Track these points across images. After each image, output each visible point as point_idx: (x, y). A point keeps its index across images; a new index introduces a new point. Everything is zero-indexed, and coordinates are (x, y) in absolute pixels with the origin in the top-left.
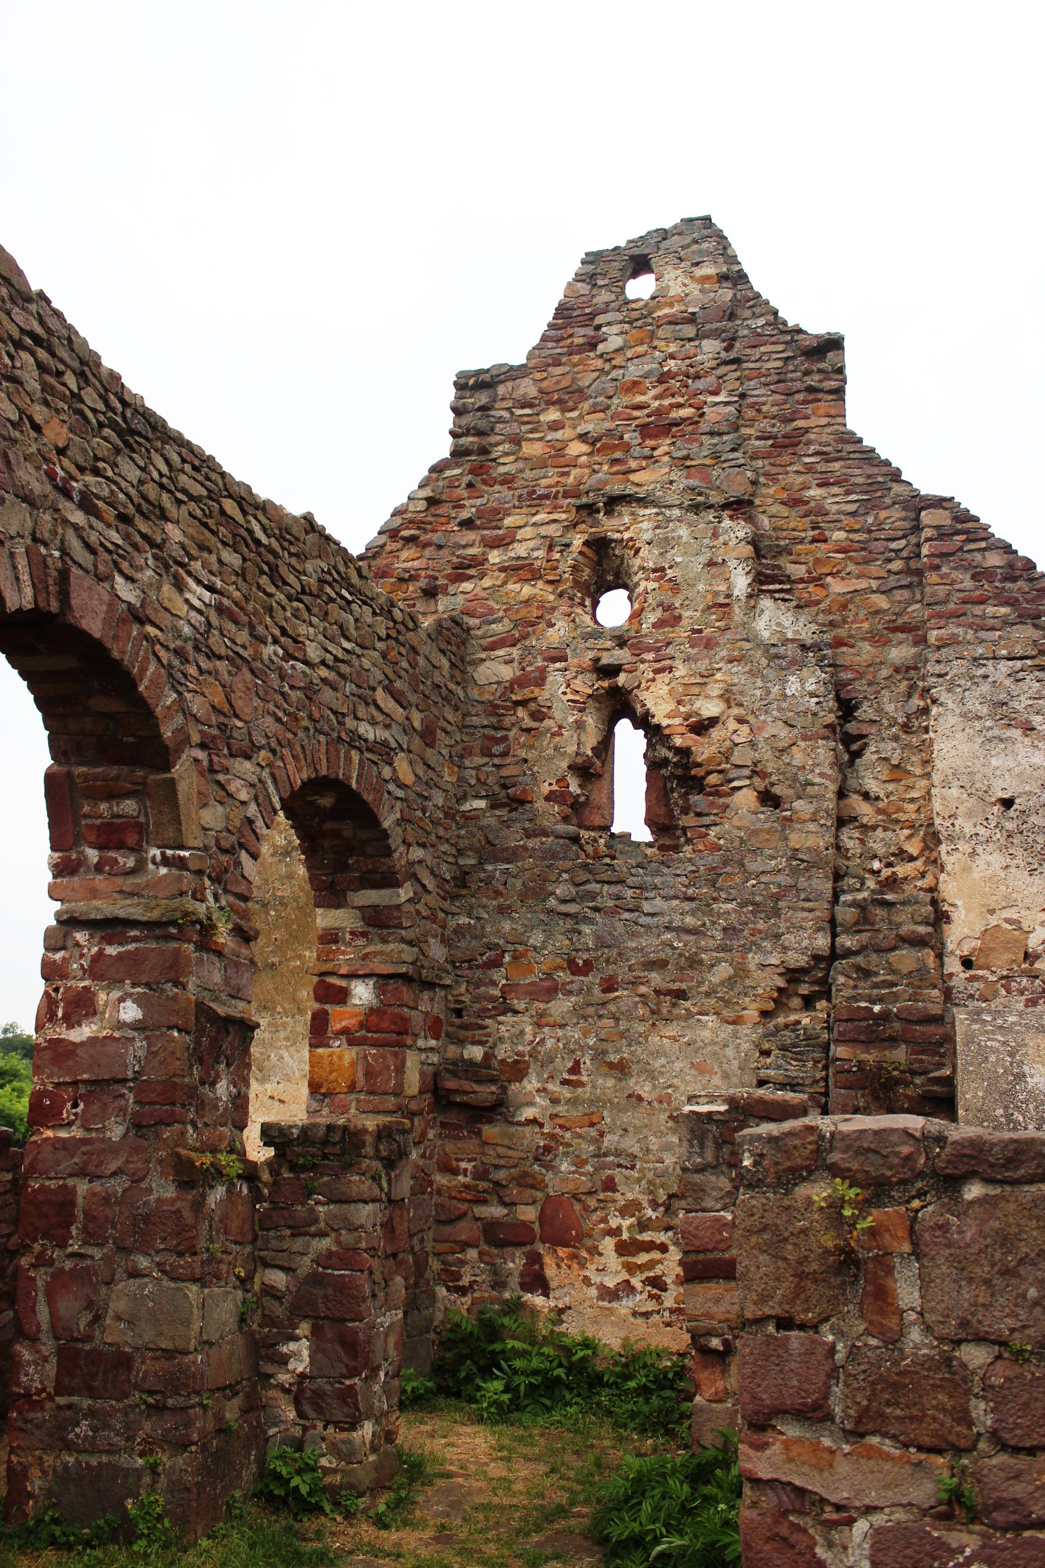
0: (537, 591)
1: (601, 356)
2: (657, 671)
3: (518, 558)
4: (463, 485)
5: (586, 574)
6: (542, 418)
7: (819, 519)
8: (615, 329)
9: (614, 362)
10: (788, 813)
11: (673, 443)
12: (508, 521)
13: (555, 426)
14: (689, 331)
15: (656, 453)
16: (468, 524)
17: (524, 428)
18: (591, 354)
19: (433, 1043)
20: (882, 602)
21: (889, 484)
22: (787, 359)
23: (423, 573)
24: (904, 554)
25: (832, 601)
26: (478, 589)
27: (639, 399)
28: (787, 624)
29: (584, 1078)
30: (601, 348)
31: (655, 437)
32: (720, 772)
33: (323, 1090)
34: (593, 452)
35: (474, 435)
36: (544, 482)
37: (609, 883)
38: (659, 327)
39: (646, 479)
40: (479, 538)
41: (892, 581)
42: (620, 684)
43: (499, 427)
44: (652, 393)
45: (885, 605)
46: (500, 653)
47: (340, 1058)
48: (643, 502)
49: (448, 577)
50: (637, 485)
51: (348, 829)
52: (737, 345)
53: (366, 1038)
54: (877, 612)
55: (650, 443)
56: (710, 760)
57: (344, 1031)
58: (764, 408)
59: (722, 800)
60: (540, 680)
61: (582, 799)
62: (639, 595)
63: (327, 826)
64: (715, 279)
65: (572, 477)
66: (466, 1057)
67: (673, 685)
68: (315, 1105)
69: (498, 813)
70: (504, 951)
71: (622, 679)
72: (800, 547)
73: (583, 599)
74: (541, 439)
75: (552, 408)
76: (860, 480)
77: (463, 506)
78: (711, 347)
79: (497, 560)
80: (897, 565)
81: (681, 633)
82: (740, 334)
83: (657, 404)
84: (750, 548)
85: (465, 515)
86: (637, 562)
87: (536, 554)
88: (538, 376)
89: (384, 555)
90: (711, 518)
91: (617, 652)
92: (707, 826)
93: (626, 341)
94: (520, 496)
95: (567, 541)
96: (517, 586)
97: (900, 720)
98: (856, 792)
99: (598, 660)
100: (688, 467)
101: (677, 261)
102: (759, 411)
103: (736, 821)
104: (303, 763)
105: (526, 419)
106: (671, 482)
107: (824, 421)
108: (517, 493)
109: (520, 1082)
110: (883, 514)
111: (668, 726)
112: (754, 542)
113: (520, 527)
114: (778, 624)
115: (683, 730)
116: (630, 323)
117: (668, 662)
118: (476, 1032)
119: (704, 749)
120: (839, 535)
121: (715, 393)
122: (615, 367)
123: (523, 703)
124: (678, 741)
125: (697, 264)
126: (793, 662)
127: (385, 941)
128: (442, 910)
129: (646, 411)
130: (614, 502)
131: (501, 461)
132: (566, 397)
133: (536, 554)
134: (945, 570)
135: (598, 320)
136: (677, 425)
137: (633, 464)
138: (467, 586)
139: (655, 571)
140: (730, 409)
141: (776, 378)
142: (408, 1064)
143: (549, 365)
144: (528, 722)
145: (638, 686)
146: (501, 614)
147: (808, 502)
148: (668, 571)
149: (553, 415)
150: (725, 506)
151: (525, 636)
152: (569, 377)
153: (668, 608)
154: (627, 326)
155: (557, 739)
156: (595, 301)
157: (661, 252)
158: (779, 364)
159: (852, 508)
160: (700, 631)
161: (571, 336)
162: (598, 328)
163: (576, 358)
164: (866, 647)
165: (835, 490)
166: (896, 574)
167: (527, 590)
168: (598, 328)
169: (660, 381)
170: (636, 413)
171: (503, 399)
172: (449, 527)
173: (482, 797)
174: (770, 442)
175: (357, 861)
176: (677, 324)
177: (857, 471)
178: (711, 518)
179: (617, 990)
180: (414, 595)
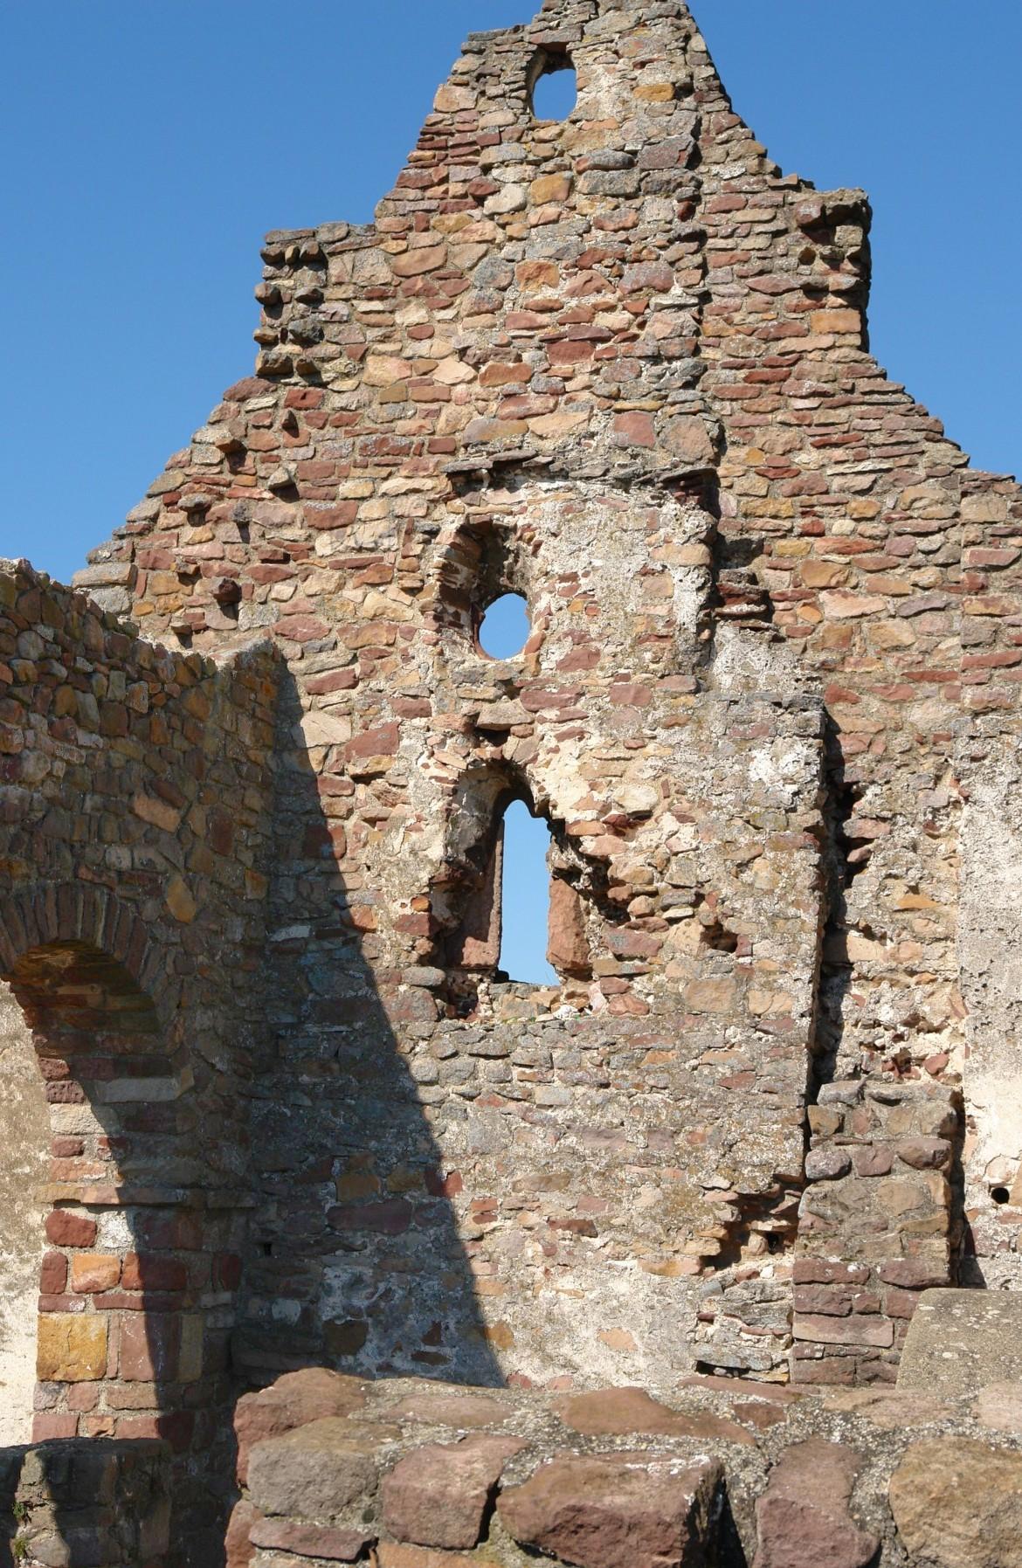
0: (388, 602)
1: (491, 217)
2: (561, 737)
3: (360, 550)
4: (277, 425)
5: (463, 576)
6: (398, 318)
7: (814, 500)
8: (511, 173)
9: (510, 230)
10: (747, 960)
11: (597, 372)
12: (346, 488)
13: (420, 333)
14: (628, 181)
15: (569, 386)
16: (286, 491)
17: (372, 334)
18: (477, 213)
19: (225, 1297)
20: (902, 632)
21: (927, 445)
22: (777, 234)
23: (216, 565)
24: (940, 558)
25: (828, 630)
26: (300, 595)
27: (547, 294)
28: (758, 666)
29: (447, 1351)
30: (490, 203)
31: (570, 357)
32: (653, 894)
33: (58, 1377)
34: (475, 378)
35: (294, 342)
36: (401, 426)
37: (487, 1057)
38: (580, 173)
39: (551, 432)
40: (301, 513)
41: (918, 600)
42: (507, 756)
43: (330, 331)
44: (567, 285)
45: (907, 638)
46: (334, 697)
47: (84, 1328)
48: (544, 471)
49: (254, 573)
50: (541, 437)
51: (92, 994)
52: (700, 209)
53: (123, 1299)
54: (897, 648)
55: (562, 367)
56: (636, 875)
57: (93, 1290)
58: (737, 317)
59: (654, 936)
60: (390, 743)
61: (454, 924)
62: (540, 614)
63: (62, 991)
64: (669, 94)
65: (443, 418)
66: (276, 1316)
67: (585, 758)
68: (46, 1400)
69: (327, 945)
70: (334, 1157)
71: (510, 748)
72: (783, 542)
73: (457, 615)
74: (397, 354)
75: (414, 301)
76: (878, 438)
77: (277, 460)
78: (659, 210)
79: (328, 551)
80: (928, 575)
81: (599, 678)
82: (705, 188)
83: (574, 302)
84: (703, 548)
85: (279, 477)
86: (537, 563)
87: (386, 543)
88: (394, 246)
89: (157, 531)
90: (648, 499)
91: (506, 705)
92: (631, 977)
93: (526, 194)
94: (364, 448)
95: (434, 526)
96: (359, 593)
97: (921, 818)
98: (856, 927)
99: (477, 715)
100: (619, 411)
101: (611, 56)
102: (729, 321)
103: (673, 970)
104: (21, 928)
105: (373, 318)
106: (592, 435)
107: (827, 341)
108: (360, 441)
109: (354, 1354)
110: (911, 493)
111: (577, 822)
112: (713, 540)
113: (363, 499)
114: (745, 666)
115: (597, 827)
116: (536, 163)
117: (577, 724)
118: (296, 1278)
119: (628, 860)
120: (841, 526)
121: (665, 290)
122: (511, 239)
123: (365, 779)
124: (589, 846)
125: (643, 65)
126: (763, 729)
127: (150, 1152)
128: (241, 1094)
129: (557, 316)
130: (505, 473)
131: (335, 386)
132: (437, 284)
133: (386, 543)
134: (992, 593)
135: (484, 159)
136: (604, 340)
137: (536, 403)
138: (283, 589)
139: (563, 579)
140: (686, 317)
141: (757, 265)
142: (185, 1334)
143: (410, 229)
144: (376, 809)
145: (534, 759)
146: (334, 635)
147: (799, 473)
148: (583, 581)
149: (413, 314)
150: (670, 483)
151: (370, 674)
152: (440, 250)
153: (581, 638)
154: (529, 170)
155: (414, 836)
156: (482, 122)
157: (587, 40)
158: (762, 242)
159: (865, 482)
160: (626, 677)
161: (445, 180)
162: (487, 169)
163: (452, 219)
164: (874, 704)
165: (838, 453)
166: (925, 589)
167: (373, 600)
168: (487, 169)
169: (579, 266)
170: (544, 318)
171: (340, 284)
172: (256, 493)
173: (303, 921)
174: (742, 374)
175: (110, 1038)
176: (606, 169)
177: (874, 424)
178: (648, 499)
179: (494, 1218)
180: (202, 601)
